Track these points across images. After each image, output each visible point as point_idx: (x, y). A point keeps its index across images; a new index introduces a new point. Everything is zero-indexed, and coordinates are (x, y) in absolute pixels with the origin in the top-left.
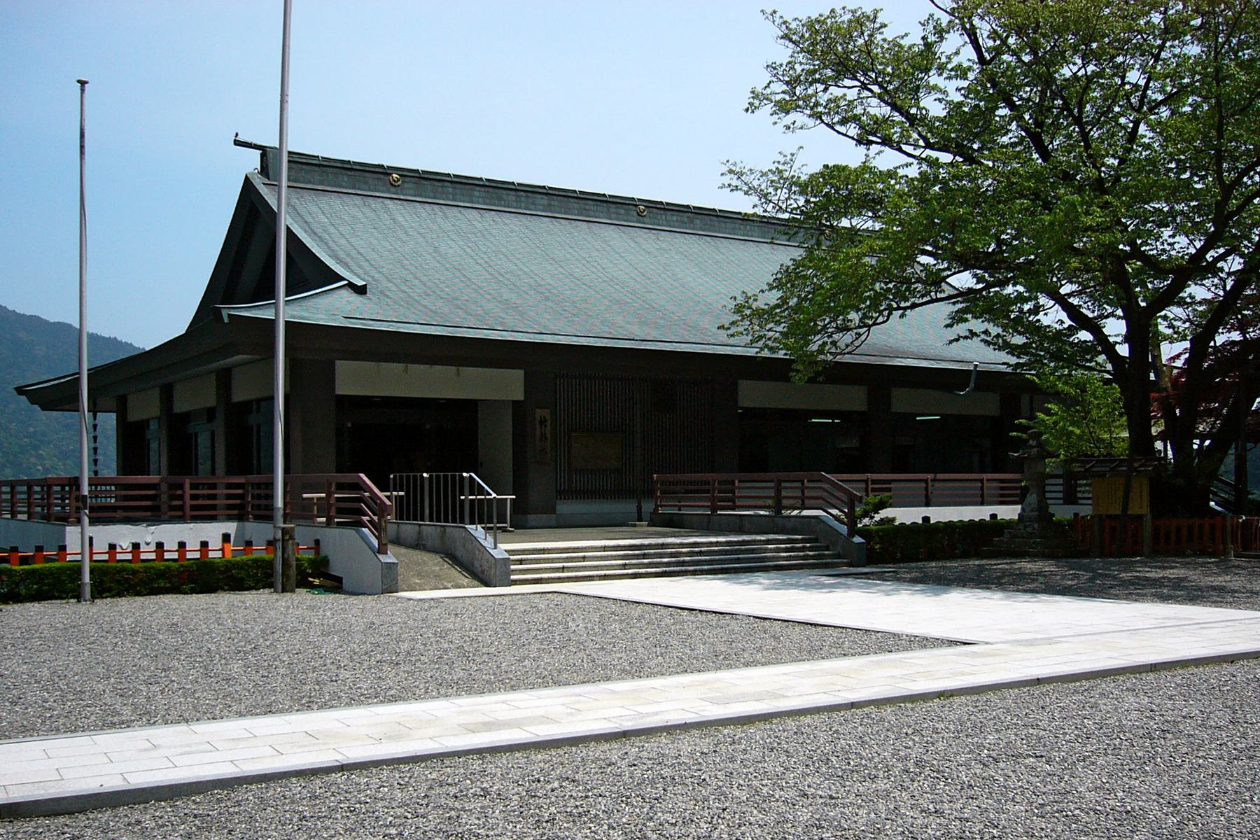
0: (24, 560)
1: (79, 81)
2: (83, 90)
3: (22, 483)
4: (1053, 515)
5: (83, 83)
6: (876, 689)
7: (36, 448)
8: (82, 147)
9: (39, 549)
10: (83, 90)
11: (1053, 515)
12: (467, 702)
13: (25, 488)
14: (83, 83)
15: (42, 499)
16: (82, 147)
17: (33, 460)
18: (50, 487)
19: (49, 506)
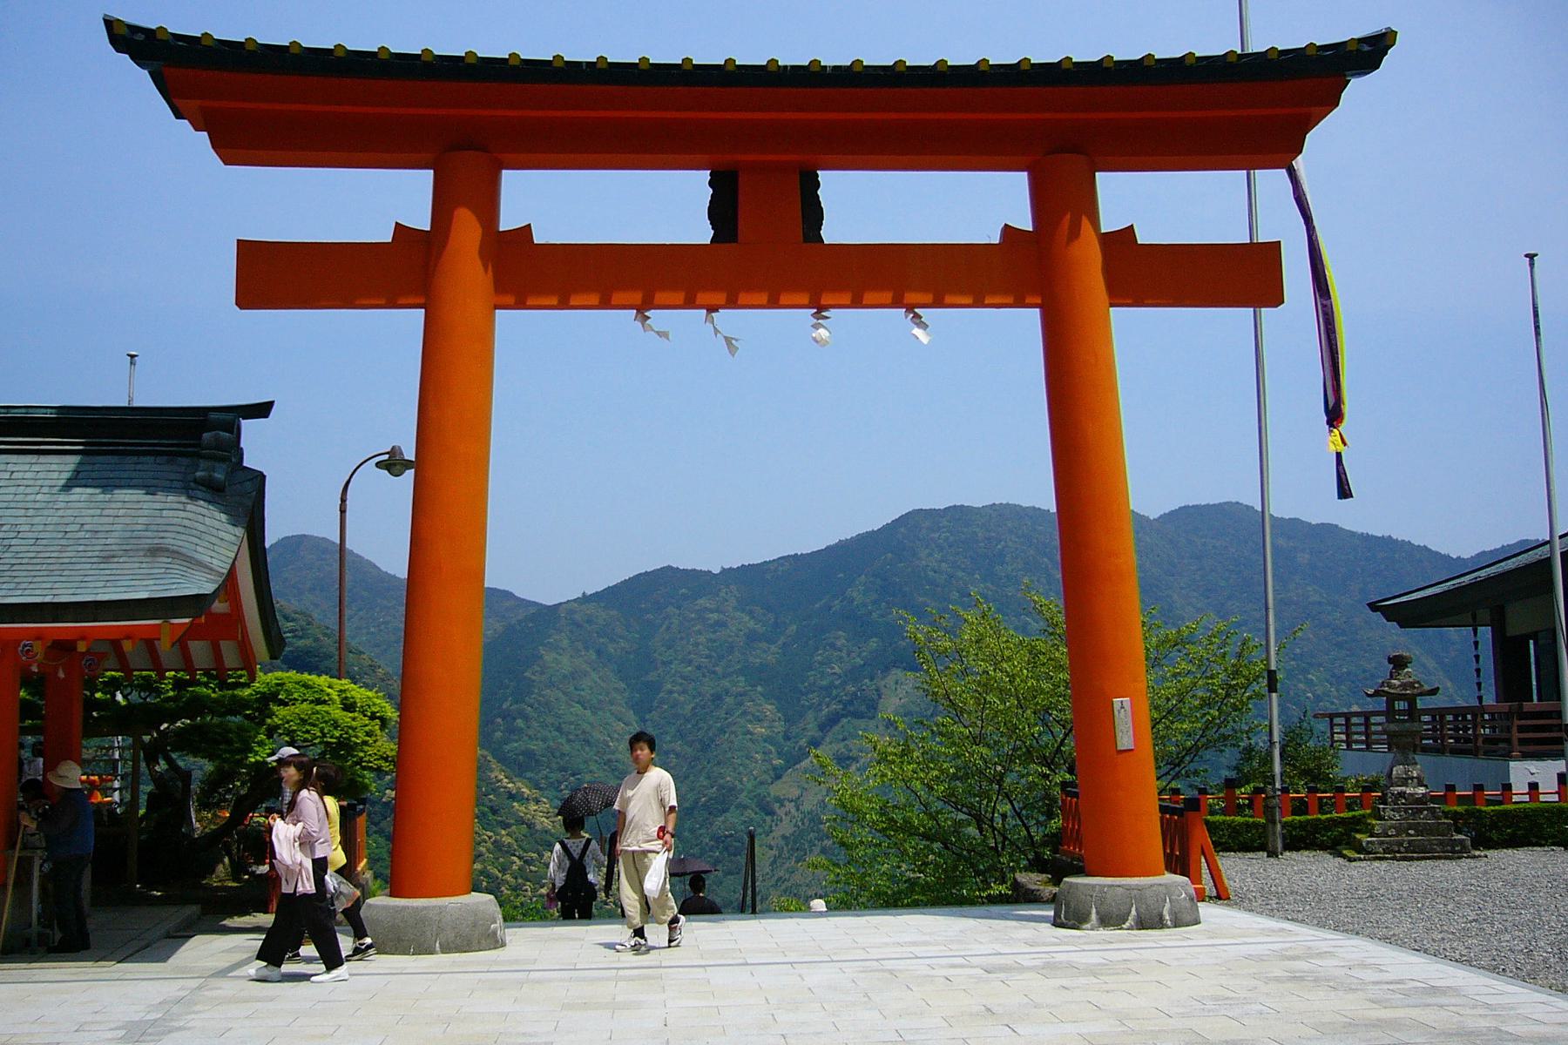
0: (1462, 800)
1: (271, 404)
2: (1532, 265)
3: (1357, 714)
4: (1008, 231)
5: (1531, 257)
6: (1348, 942)
7: (1305, 671)
8: (1537, 327)
9: (1479, 788)
10: (1532, 265)
11: (1008, 231)
12: (1305, 935)
13: (1362, 720)
14: (1531, 257)
15: (1434, 729)
16: (1537, 327)
17: (1301, 686)
18: (1442, 717)
19: (1443, 738)
